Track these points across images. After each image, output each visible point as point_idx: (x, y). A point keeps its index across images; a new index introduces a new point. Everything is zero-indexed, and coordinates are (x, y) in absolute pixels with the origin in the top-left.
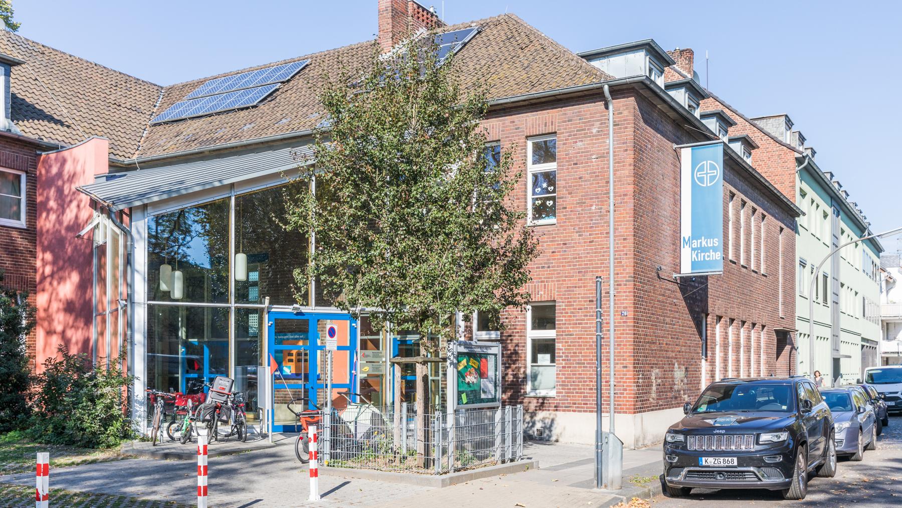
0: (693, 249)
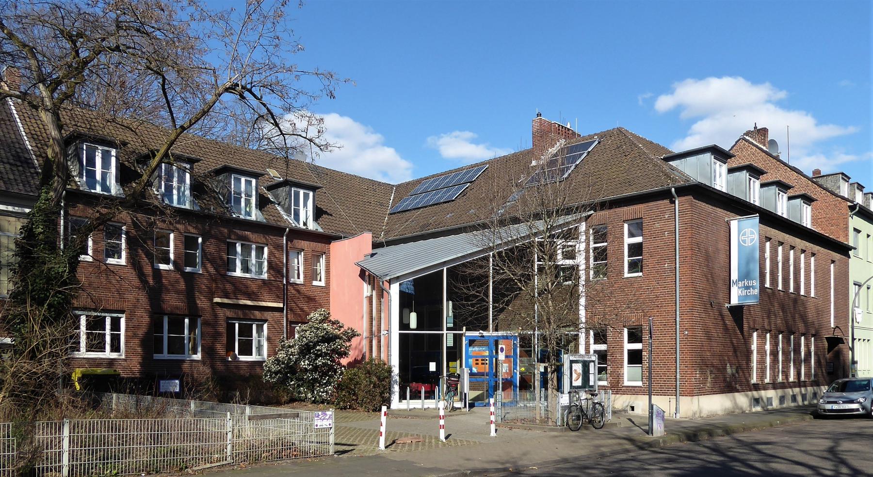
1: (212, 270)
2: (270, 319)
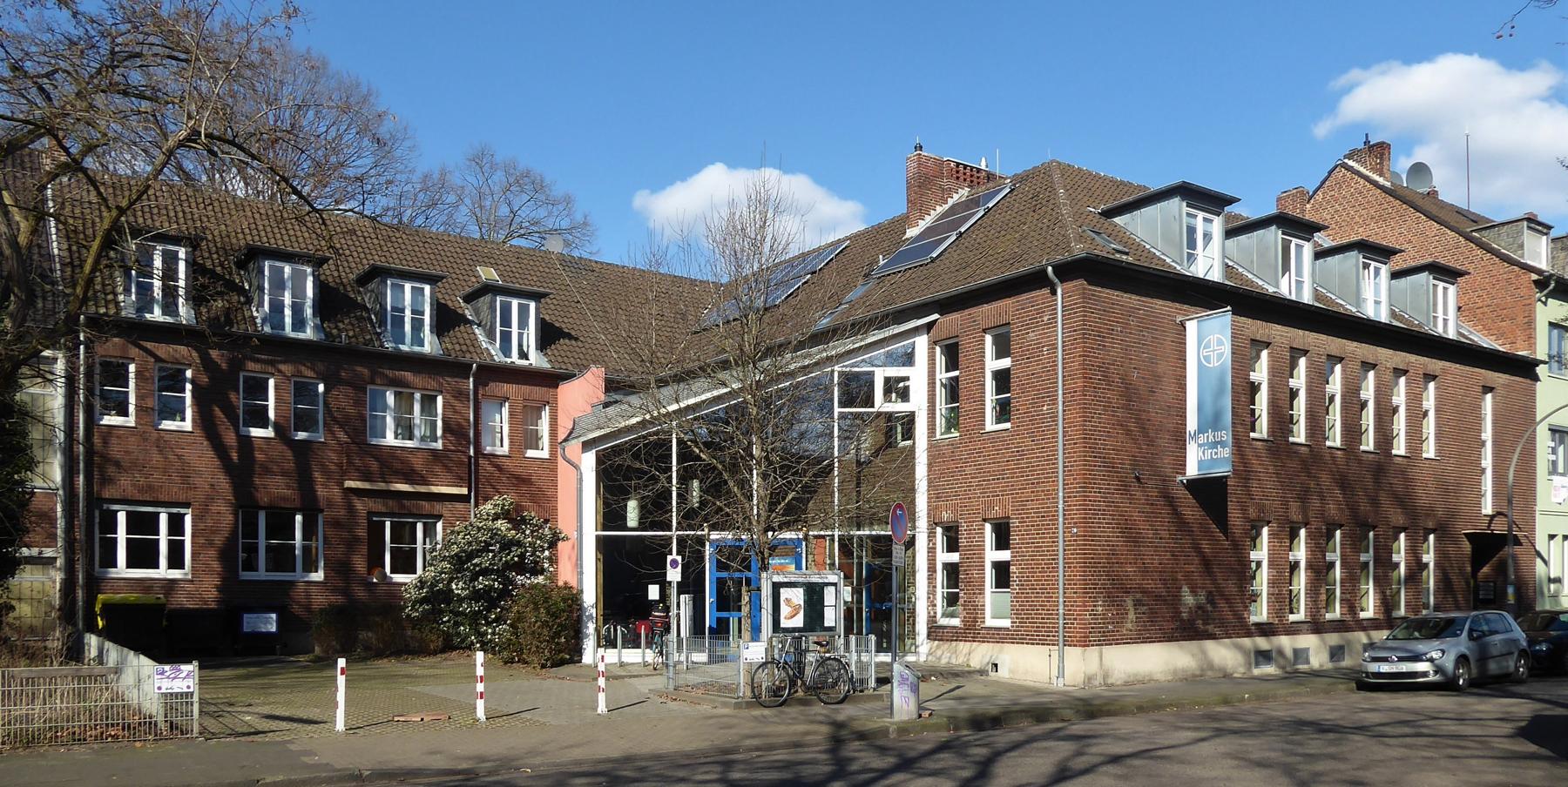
1: (342, 436)
2: (446, 513)
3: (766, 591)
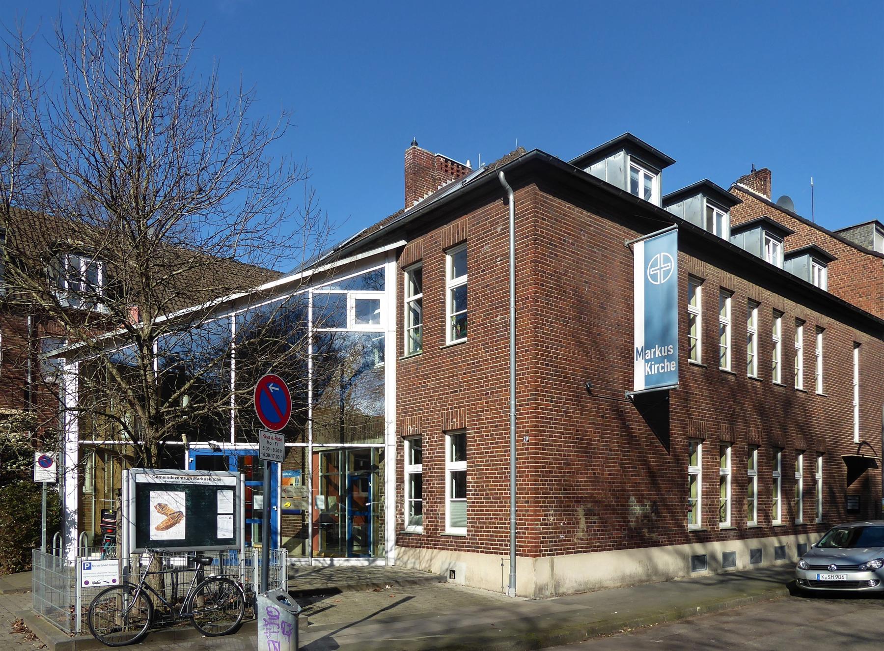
0: (647, 361)
3: (128, 494)
